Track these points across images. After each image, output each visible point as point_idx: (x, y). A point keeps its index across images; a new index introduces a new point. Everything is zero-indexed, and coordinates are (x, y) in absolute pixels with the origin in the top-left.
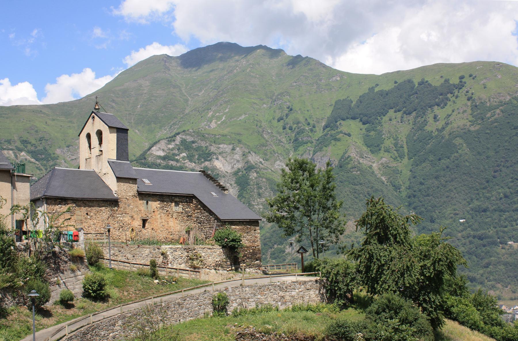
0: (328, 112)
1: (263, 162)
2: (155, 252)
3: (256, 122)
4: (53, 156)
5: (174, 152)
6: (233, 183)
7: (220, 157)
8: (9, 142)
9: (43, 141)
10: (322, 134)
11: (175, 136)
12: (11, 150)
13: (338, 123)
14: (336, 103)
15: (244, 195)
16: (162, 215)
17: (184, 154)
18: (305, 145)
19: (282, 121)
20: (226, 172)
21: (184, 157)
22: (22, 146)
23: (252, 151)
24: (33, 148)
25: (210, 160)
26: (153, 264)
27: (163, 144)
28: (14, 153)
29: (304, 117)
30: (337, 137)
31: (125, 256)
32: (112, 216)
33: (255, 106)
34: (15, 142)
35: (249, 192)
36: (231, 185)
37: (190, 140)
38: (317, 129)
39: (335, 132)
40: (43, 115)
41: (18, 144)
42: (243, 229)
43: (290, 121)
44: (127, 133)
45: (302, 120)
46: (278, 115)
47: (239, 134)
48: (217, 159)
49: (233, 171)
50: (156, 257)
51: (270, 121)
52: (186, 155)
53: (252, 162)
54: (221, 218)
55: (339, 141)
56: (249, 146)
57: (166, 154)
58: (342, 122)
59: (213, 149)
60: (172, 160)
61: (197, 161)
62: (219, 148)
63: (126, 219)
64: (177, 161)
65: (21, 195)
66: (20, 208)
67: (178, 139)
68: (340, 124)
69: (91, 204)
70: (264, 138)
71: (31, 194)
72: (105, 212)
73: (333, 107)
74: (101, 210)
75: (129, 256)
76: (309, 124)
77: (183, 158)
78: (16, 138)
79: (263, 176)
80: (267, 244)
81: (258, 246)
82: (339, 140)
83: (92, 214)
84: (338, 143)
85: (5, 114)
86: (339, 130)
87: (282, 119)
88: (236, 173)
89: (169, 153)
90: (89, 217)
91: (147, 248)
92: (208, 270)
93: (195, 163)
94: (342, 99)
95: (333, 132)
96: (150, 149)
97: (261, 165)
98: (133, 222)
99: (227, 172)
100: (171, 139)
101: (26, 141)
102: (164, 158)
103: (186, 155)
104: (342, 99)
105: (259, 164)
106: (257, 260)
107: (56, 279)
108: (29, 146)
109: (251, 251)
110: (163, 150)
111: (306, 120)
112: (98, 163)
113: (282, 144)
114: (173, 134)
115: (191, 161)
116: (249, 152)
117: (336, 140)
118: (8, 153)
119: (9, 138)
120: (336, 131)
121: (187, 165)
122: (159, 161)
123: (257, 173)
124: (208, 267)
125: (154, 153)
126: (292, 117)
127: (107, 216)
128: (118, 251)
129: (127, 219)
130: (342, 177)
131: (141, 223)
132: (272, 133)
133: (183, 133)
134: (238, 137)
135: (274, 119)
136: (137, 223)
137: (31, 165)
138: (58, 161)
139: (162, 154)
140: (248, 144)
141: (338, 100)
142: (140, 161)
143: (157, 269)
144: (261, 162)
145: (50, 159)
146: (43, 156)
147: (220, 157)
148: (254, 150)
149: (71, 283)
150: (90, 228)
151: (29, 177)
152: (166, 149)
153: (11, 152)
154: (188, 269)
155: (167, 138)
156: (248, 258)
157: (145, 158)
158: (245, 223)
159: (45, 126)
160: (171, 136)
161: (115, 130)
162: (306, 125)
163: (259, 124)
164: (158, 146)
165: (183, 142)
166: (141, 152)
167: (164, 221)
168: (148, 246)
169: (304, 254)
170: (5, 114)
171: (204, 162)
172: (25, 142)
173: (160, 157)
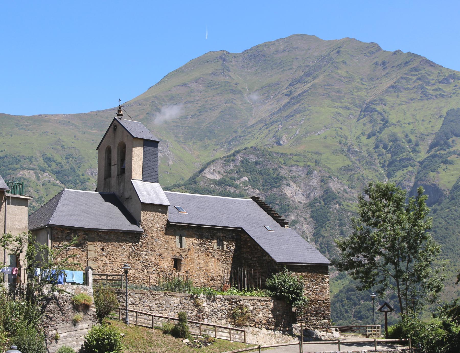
0: (438, 125)
1: (348, 190)
2: (186, 302)
3: (339, 138)
4: (82, 177)
5: (232, 175)
6: (308, 216)
7: (292, 183)
8: (30, 159)
9: (71, 159)
10: (428, 155)
11: (234, 155)
12: (33, 169)
13: (450, 140)
14: (447, 113)
15: (322, 233)
16: (200, 253)
17: (246, 178)
18: (405, 169)
19: (373, 138)
20: (299, 202)
21: (246, 181)
22: (45, 165)
23: (333, 175)
24: (58, 168)
25: (278, 187)
26: (181, 319)
27: (217, 167)
28: (35, 173)
29: (404, 132)
30: (449, 159)
31: (147, 306)
32: (134, 252)
33: (340, 119)
34: (37, 160)
35: (328, 228)
36: (305, 219)
37: (253, 160)
38: (421, 147)
39: (446, 152)
40: (71, 127)
41: (41, 162)
42: (307, 276)
43: (385, 135)
44: (157, 147)
45: (400, 136)
46: (369, 129)
47: (317, 153)
48: (288, 185)
49: (308, 201)
50: (188, 309)
51: (359, 137)
52: (247, 180)
53: (333, 189)
54: (277, 261)
55: (451, 164)
56: (329, 169)
57: (222, 177)
58: (454, 138)
59: (283, 172)
60: (230, 186)
61: (261, 188)
62: (291, 171)
63: (153, 258)
64: (236, 186)
65: (17, 223)
66: (11, 239)
67: (239, 157)
68: (453, 141)
69: (107, 237)
70: (351, 160)
71: (30, 223)
72: (125, 249)
73: (443, 119)
74: (120, 245)
75: (153, 306)
76: (410, 141)
77: (245, 182)
78: (38, 155)
79: (347, 208)
80: (351, 299)
81: (326, 299)
82: (451, 163)
83: (109, 250)
84: (449, 167)
85: (26, 126)
86: (452, 150)
87: (374, 135)
88: (311, 205)
89: (226, 176)
90: (104, 254)
91: (176, 296)
92: (257, 329)
93: (259, 190)
94: (455, 109)
95: (442, 152)
96: (202, 171)
97: (345, 194)
98: (162, 262)
99: (301, 203)
100: (228, 160)
101: (50, 159)
102: (219, 183)
103: (247, 180)
104: (455, 109)
105: (342, 192)
106: (324, 319)
107: (54, 332)
108: (54, 165)
109: (317, 306)
110: (219, 172)
111: (407, 136)
112: (119, 184)
113: (374, 167)
114: (232, 152)
115: (254, 187)
116: (330, 177)
117: (446, 162)
118: (28, 174)
119: (30, 155)
120: (447, 150)
121: (249, 192)
122: (213, 186)
123: (339, 205)
124: (257, 325)
125: (208, 176)
126: (386, 131)
127: (127, 253)
128: (138, 299)
129: (153, 258)
130: (455, 213)
131: (171, 263)
132: (361, 152)
133: (244, 152)
134: (316, 157)
135: (363, 134)
136: (167, 264)
137: (56, 188)
138: (88, 184)
139: (217, 177)
140: (328, 166)
141: (451, 110)
142: (190, 186)
143: (188, 324)
144: (345, 191)
145: (78, 181)
146: (70, 178)
147: (292, 183)
148: (336, 174)
149: (74, 338)
150: (105, 268)
151: (27, 199)
152: (222, 171)
153: (32, 172)
154: (229, 326)
155: (224, 157)
156: (313, 315)
157: (195, 183)
158: (309, 268)
159: (73, 141)
160: (229, 154)
161: (142, 142)
162: (406, 143)
163: (343, 141)
164: (212, 167)
165: (245, 162)
166: (191, 175)
167: (201, 261)
168: (177, 294)
169: (388, 313)
170: (26, 126)
171: (271, 188)
172: (48, 160)
173: (214, 182)
